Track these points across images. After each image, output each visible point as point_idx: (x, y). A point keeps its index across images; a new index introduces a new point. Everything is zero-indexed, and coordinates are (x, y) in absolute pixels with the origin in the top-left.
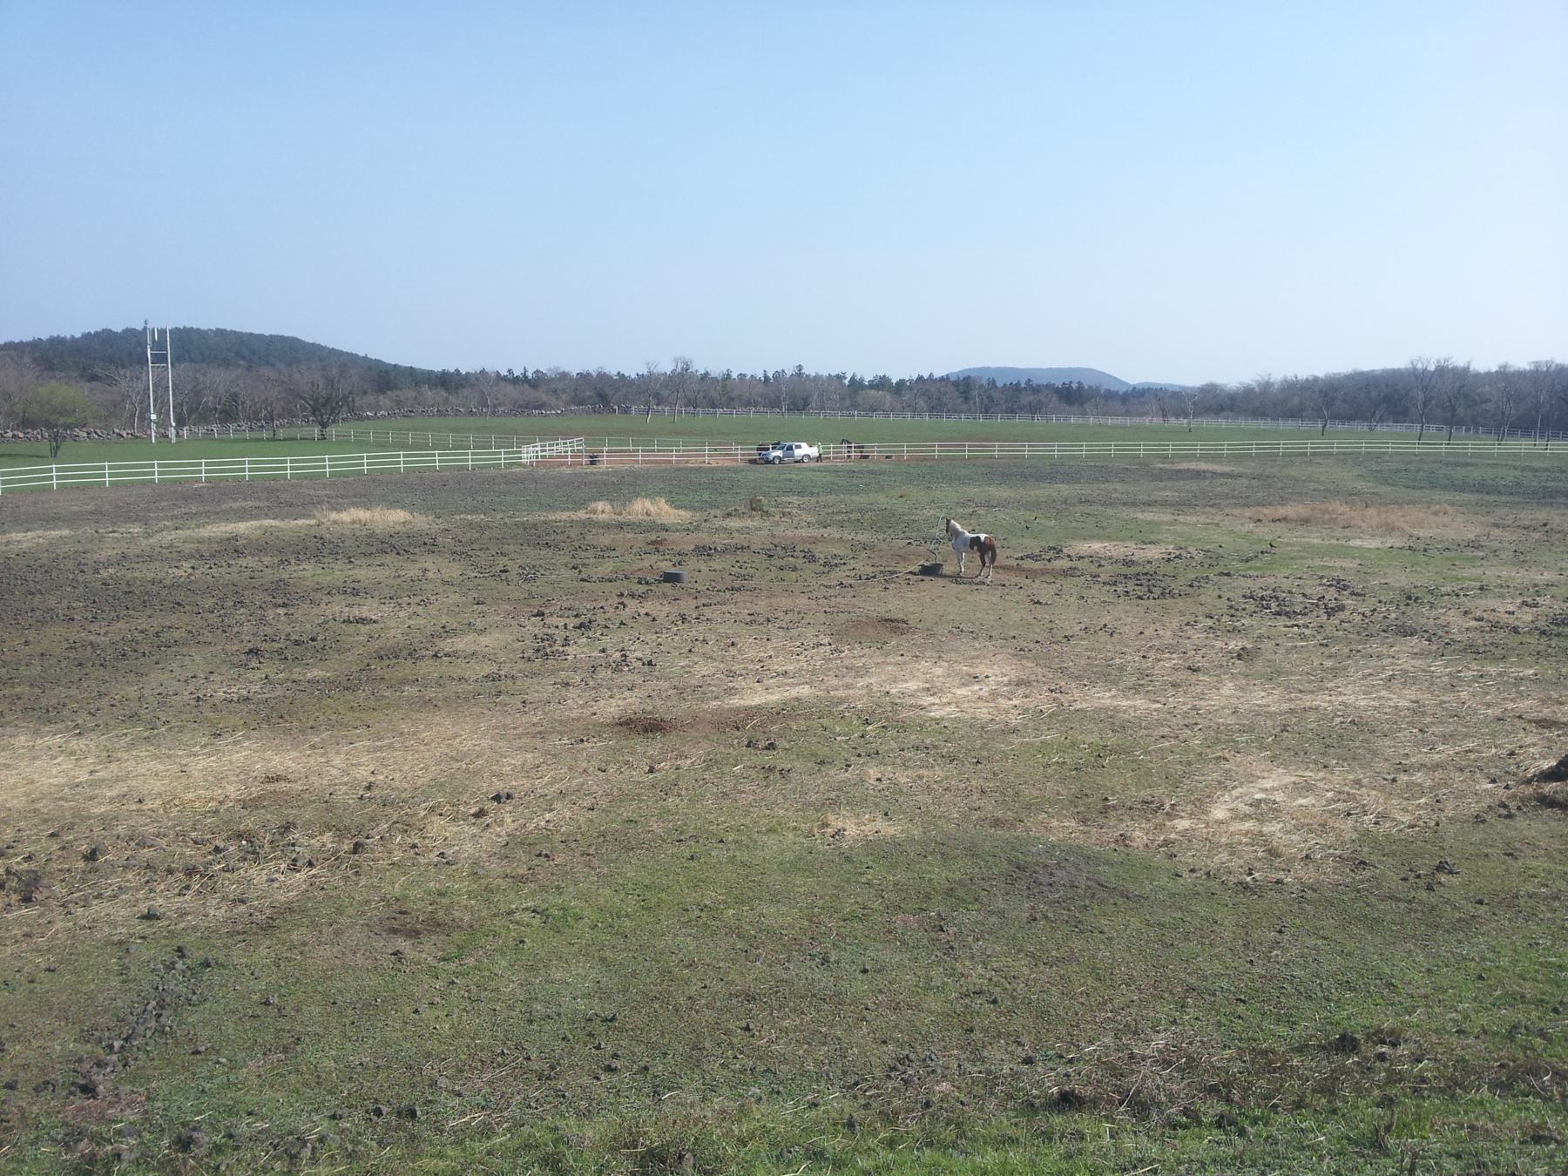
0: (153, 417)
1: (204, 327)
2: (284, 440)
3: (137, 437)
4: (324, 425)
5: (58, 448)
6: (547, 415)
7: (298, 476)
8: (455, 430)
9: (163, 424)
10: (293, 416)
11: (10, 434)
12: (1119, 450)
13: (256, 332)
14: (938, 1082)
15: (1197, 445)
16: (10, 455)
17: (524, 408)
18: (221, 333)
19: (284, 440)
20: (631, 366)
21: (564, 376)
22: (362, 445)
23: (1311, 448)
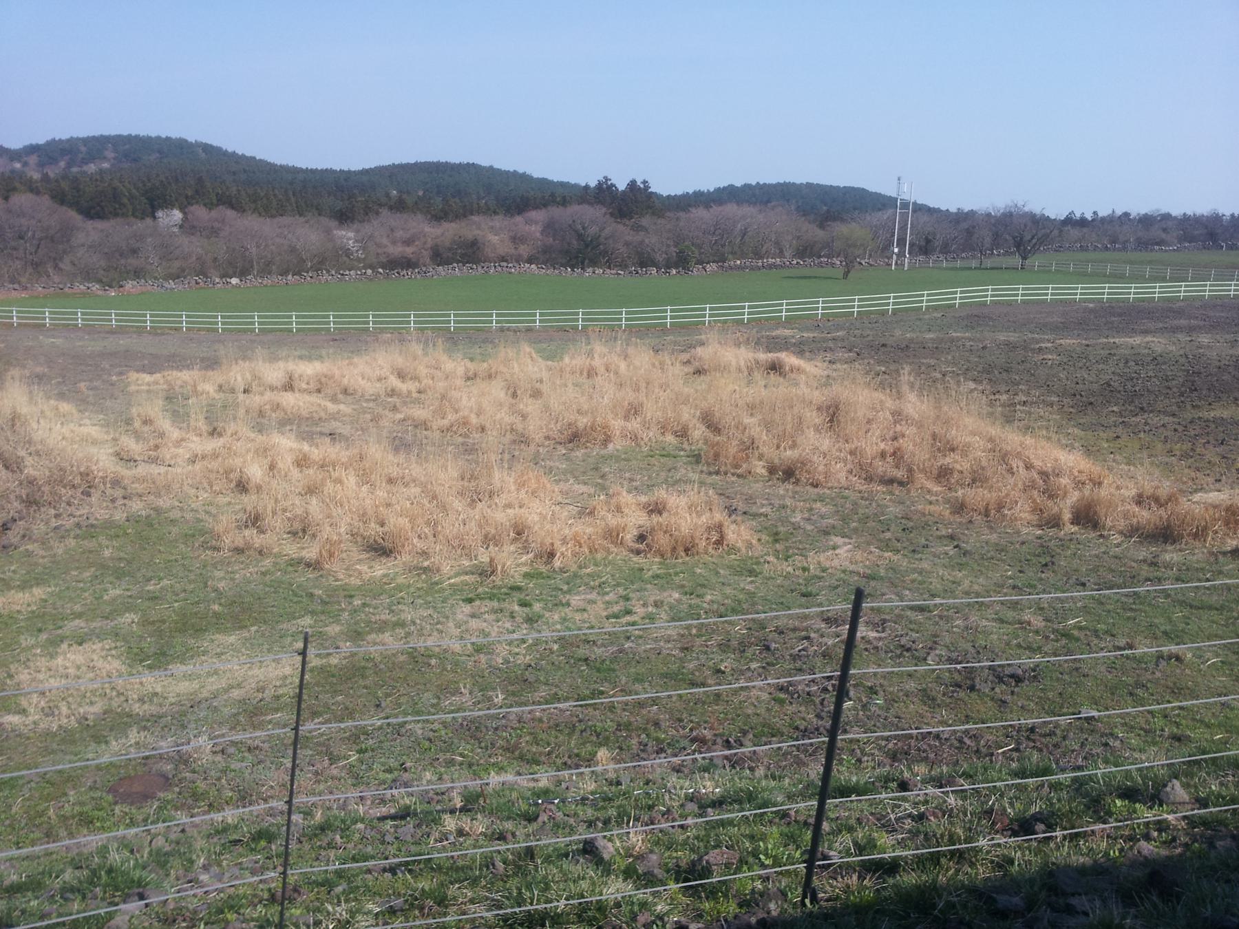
0: (896, 250)
1: (798, 181)
2: (992, 269)
3: (871, 265)
4: (1024, 258)
5: (849, 272)
6: (1166, 251)
7: (1085, 301)
8: (1131, 263)
9: (901, 255)
10: (974, 250)
11: (795, 262)
12: (1189, 291)
13: (835, 184)
14: (173, 800)
15: (1104, 288)
16: (816, 277)
17: (1144, 245)
18: (809, 185)
19: (992, 269)
20: (1056, 210)
21: (1167, 217)
22: (1083, 276)
23: (992, 296)
